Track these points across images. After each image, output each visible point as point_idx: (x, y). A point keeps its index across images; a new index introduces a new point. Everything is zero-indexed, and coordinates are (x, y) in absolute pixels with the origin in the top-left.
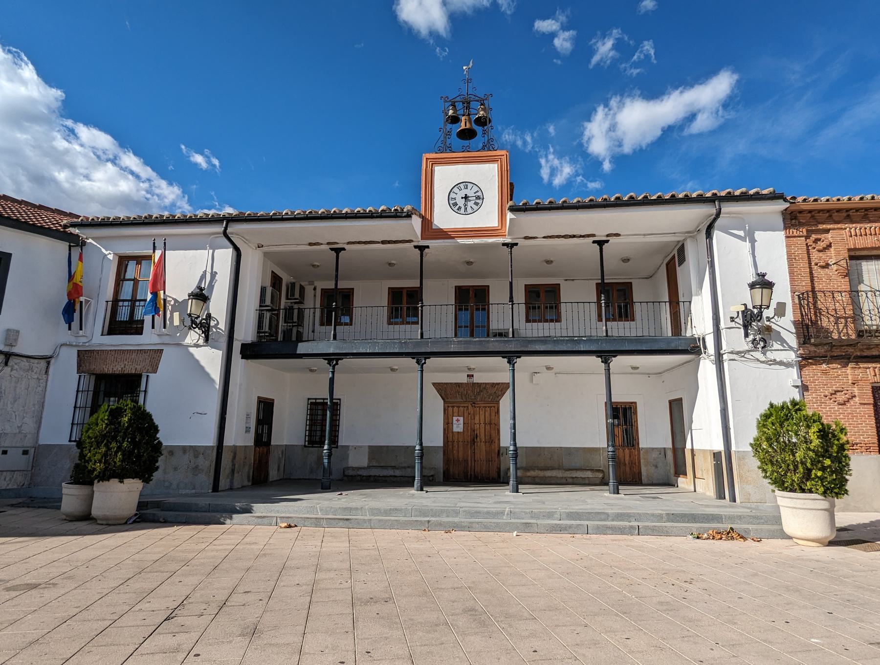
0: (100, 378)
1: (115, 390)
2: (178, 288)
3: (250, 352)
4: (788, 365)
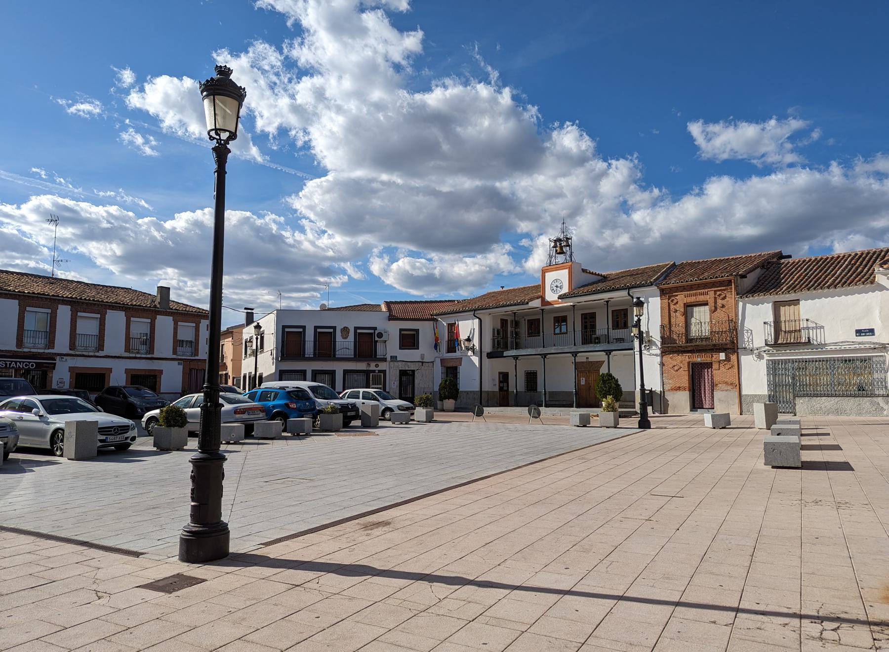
0: (447, 368)
1: (452, 372)
2: (463, 336)
3: (490, 356)
4: (656, 355)
